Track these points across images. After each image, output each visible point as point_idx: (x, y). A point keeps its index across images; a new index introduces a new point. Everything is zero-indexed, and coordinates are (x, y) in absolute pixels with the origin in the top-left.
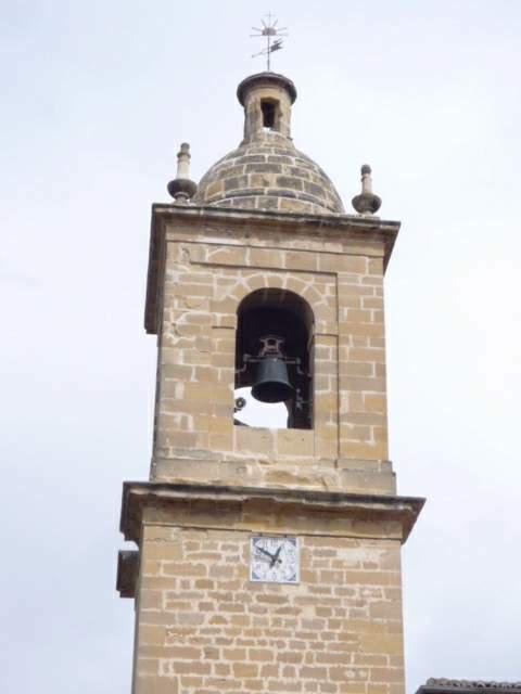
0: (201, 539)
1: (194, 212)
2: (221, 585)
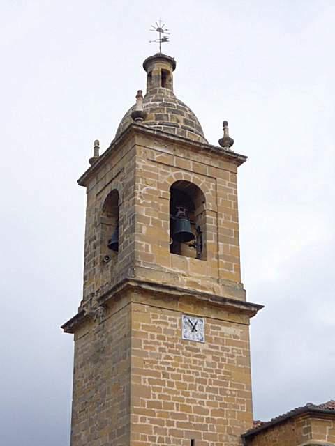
0: (159, 313)
1: (152, 132)
2: (169, 339)
